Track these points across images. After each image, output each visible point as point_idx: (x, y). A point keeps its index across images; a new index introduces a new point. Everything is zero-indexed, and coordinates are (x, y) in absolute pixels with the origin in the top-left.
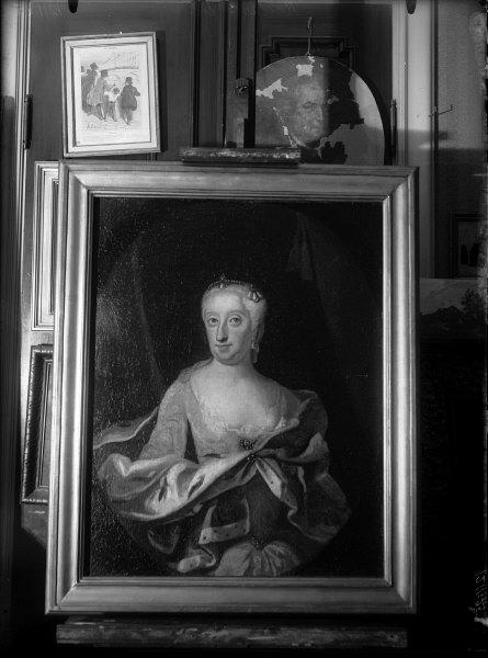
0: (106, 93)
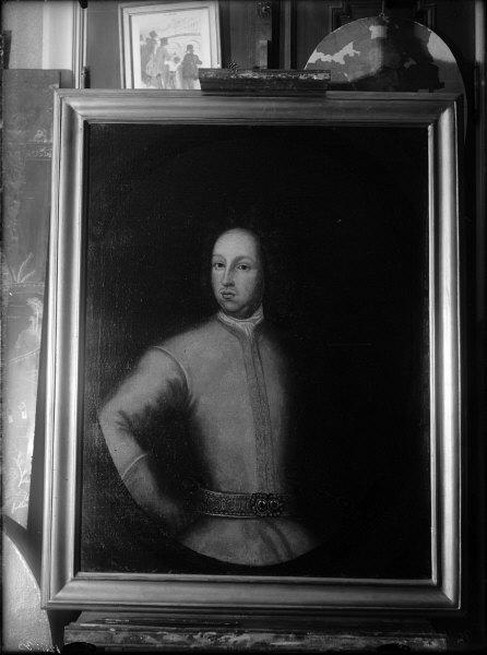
0: (166, 63)
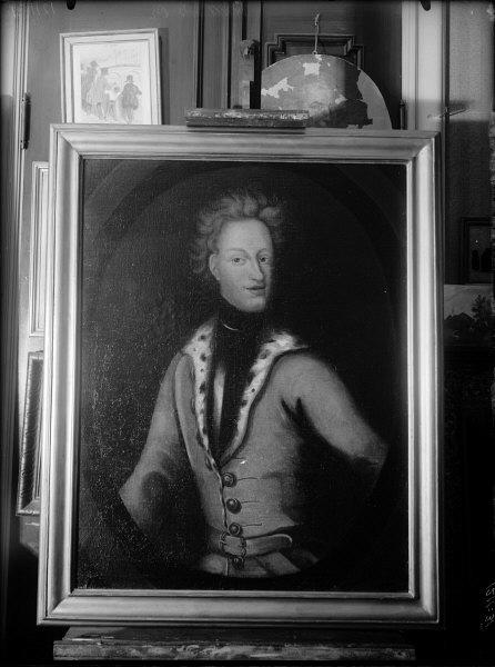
0: (106, 92)
